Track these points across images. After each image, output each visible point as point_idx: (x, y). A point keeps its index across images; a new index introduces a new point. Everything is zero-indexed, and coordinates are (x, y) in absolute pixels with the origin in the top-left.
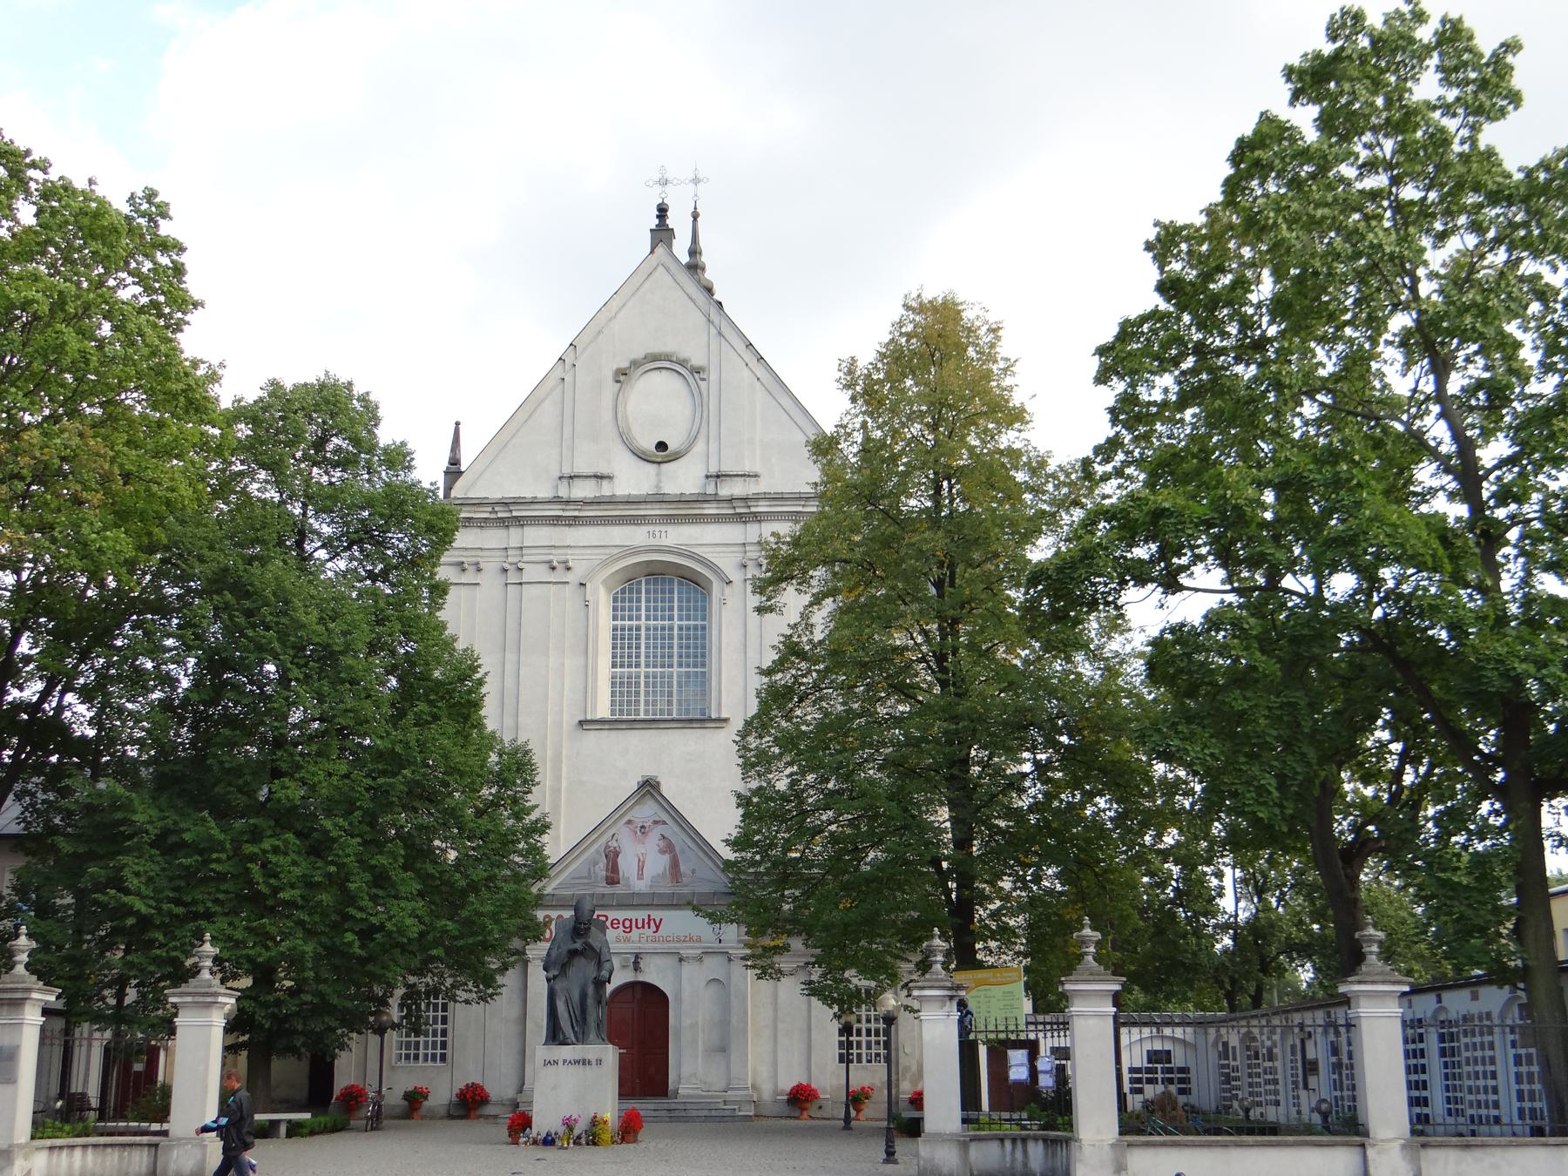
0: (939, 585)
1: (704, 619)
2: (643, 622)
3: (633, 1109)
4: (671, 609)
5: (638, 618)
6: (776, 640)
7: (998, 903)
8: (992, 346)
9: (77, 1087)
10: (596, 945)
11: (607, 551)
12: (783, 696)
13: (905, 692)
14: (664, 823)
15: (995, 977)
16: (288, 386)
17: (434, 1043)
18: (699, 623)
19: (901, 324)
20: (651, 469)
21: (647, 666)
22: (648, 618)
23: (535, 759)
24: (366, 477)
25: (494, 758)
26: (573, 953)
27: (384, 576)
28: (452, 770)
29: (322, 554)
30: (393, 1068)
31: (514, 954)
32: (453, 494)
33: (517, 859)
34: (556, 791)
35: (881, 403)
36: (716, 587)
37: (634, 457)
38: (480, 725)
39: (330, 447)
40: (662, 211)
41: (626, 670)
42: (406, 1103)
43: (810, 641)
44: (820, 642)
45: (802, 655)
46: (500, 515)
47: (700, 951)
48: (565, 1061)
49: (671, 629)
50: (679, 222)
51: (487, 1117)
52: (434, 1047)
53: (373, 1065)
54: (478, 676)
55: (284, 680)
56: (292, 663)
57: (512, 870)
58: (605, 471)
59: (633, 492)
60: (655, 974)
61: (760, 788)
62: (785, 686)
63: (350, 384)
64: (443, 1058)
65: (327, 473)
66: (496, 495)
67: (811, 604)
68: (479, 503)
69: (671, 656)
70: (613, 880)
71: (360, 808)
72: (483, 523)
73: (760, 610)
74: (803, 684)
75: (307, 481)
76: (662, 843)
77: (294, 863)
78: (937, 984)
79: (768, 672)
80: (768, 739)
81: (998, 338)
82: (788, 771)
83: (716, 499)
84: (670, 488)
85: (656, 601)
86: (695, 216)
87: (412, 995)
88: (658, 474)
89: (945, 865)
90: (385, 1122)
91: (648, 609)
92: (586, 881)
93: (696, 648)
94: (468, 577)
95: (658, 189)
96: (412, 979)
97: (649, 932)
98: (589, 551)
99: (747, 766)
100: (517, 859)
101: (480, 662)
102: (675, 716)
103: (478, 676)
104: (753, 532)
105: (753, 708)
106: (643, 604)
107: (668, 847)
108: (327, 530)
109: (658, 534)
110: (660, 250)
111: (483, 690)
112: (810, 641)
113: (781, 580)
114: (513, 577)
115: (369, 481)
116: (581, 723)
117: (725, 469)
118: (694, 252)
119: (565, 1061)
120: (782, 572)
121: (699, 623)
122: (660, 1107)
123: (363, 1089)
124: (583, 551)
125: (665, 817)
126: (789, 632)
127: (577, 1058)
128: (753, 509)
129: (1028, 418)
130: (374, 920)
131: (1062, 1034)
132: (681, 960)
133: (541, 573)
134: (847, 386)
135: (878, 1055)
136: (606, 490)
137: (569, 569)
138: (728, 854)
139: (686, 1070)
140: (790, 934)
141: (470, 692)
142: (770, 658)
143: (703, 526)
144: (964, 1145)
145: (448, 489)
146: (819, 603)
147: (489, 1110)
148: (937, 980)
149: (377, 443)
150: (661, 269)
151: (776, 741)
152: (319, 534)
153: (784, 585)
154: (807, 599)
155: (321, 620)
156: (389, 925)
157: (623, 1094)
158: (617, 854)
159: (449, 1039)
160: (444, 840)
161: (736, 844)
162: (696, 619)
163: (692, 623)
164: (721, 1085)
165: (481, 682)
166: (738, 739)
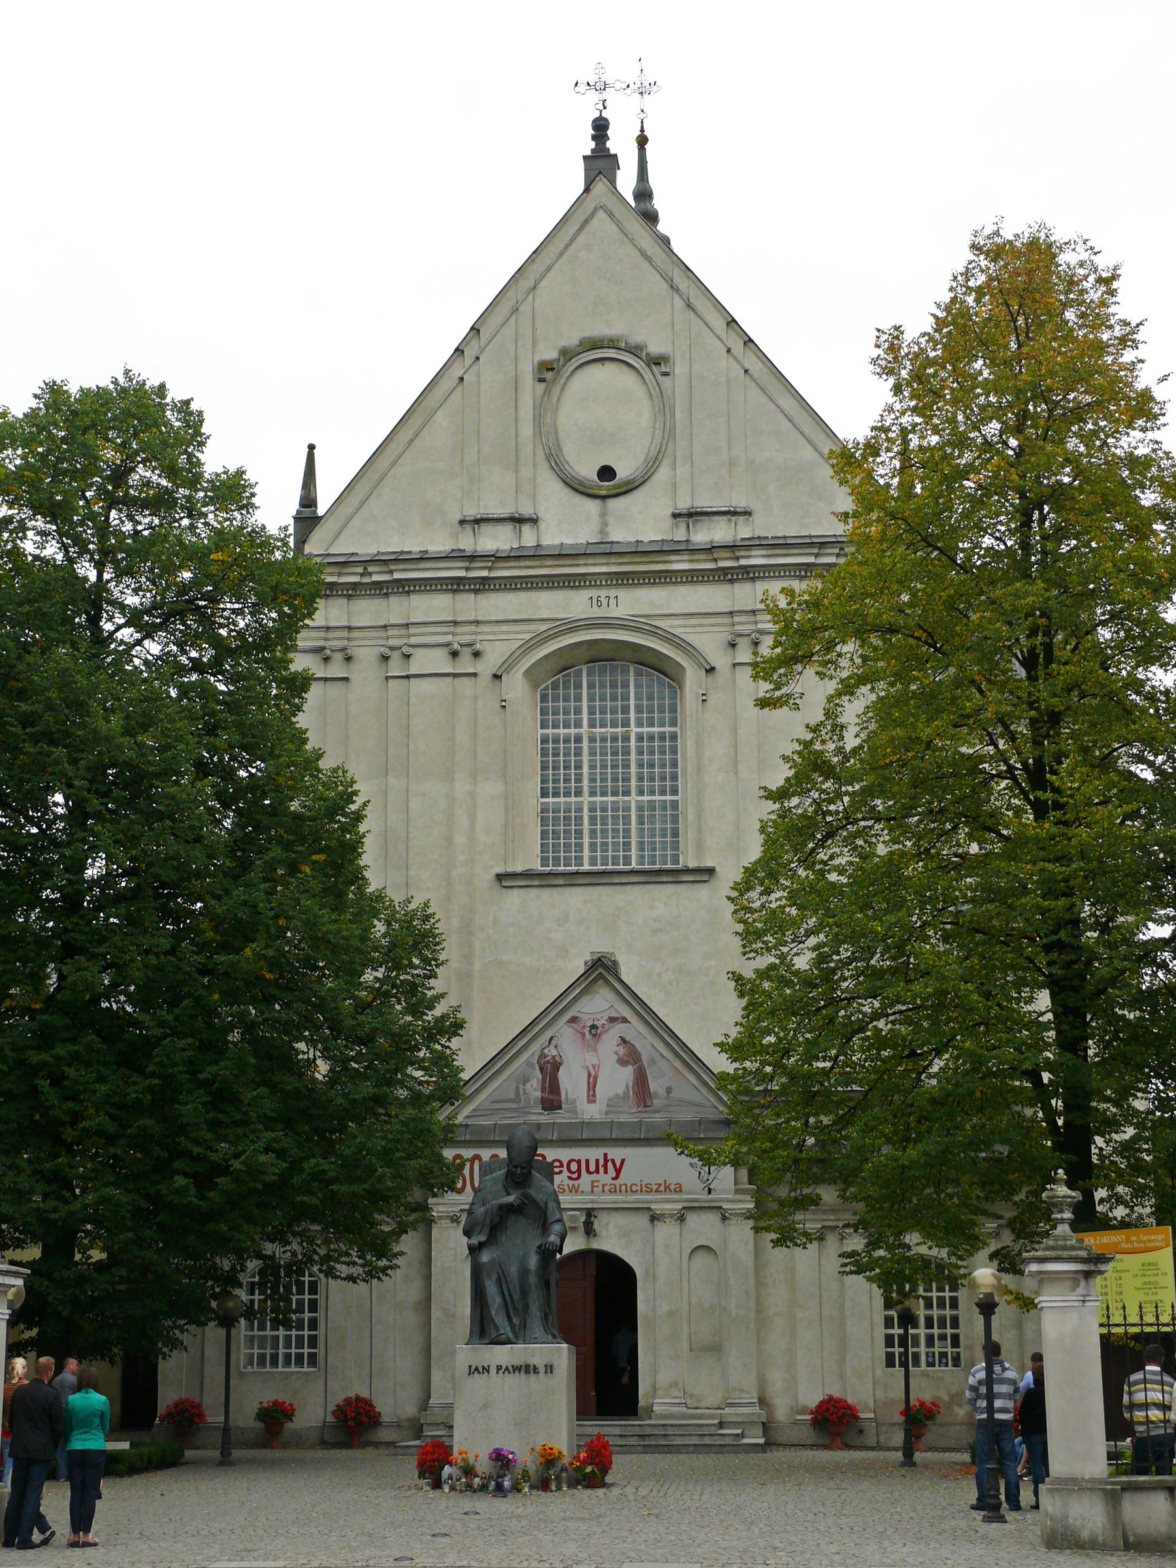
0: (1029, 663)
1: (673, 723)
2: (585, 730)
3: (599, 1436)
4: (626, 710)
5: (578, 724)
6: (791, 748)
7: (1130, 1132)
8: (1103, 304)
9: (419, 654)
10: (539, 1197)
11: (532, 627)
12: (800, 831)
13: (984, 825)
14: (625, 1020)
15: (1128, 1241)
16: (73, 389)
17: (300, 1339)
18: (667, 729)
19: (967, 274)
20: (592, 507)
21: (593, 793)
22: (592, 725)
23: (441, 927)
24: (186, 522)
25: (380, 927)
26: (508, 1211)
27: (216, 666)
28: (319, 941)
29: (126, 634)
30: (241, 1375)
31: (414, 1210)
32: (308, 549)
33: (418, 1074)
34: (465, 977)
35: (937, 395)
36: (692, 678)
37: (567, 490)
38: (358, 878)
39: (134, 479)
40: (600, 128)
41: (562, 799)
42: (260, 1425)
43: (839, 750)
44: (855, 751)
45: (828, 771)
46: (375, 578)
47: (680, 1206)
48: (499, 1368)
49: (626, 739)
50: (621, 144)
51: (377, 1445)
52: (300, 1345)
53: (214, 1370)
54: (353, 807)
55: (77, 814)
56: (89, 791)
57: (409, 1089)
58: (526, 510)
59: (567, 541)
60: (610, 1241)
61: (773, 967)
62: (804, 816)
63: (162, 388)
64: (313, 1360)
65: (131, 518)
66: (367, 549)
67: (839, 694)
68: (344, 564)
69: (627, 779)
70: (552, 1100)
71: (189, 995)
72: (352, 592)
73: (763, 703)
74: (830, 813)
75: (103, 530)
76: (622, 1050)
77: (101, 1079)
78: (1065, 1254)
79: (780, 795)
80: (779, 894)
81: (1112, 293)
82: (812, 941)
83: (693, 551)
84: (620, 535)
85: (603, 698)
86: (642, 141)
87: (270, 1267)
88: (603, 514)
89: (1046, 1077)
90: (236, 1453)
91: (591, 711)
92: (514, 1106)
93: (663, 766)
94: (336, 669)
95: (594, 97)
96: (269, 1248)
97: (605, 1178)
98: (504, 628)
99: (750, 936)
100: (418, 1074)
101: (355, 787)
102: (634, 865)
103: (353, 807)
104: (746, 595)
105: (754, 851)
106: (585, 704)
107: (630, 1056)
108: (132, 600)
109: (604, 602)
110: (600, 187)
111: (362, 828)
112: (839, 750)
113: (796, 660)
114: (395, 668)
115: (192, 527)
116: (500, 877)
117: (704, 502)
118: (644, 193)
119: (499, 1368)
120: (797, 647)
121: (667, 729)
122: (629, 1431)
123: (199, 1405)
124: (496, 628)
125: (626, 1012)
126: (809, 736)
127: (517, 1363)
128: (743, 562)
129: (1156, 410)
130: (215, 1157)
131: (1117, 1318)
132: (654, 1218)
133: (438, 661)
134: (888, 371)
135: (943, 1355)
136: (528, 537)
137: (476, 654)
138: (722, 1064)
139: (664, 1377)
140: (818, 1181)
141: (344, 829)
142: (780, 775)
143: (671, 588)
144: (1113, 1498)
145: (301, 541)
146: (852, 694)
147: (384, 1435)
148: (1064, 1248)
149: (201, 474)
150: (601, 214)
151: (792, 898)
152: (122, 607)
153: (799, 667)
154: (831, 686)
155: (129, 732)
156: (236, 1164)
157: (583, 1411)
158: (556, 1065)
159: (320, 1333)
160: (311, 1042)
161: (735, 1050)
162: (662, 725)
163: (656, 729)
164: (714, 1399)
165: (358, 817)
166: (735, 894)
